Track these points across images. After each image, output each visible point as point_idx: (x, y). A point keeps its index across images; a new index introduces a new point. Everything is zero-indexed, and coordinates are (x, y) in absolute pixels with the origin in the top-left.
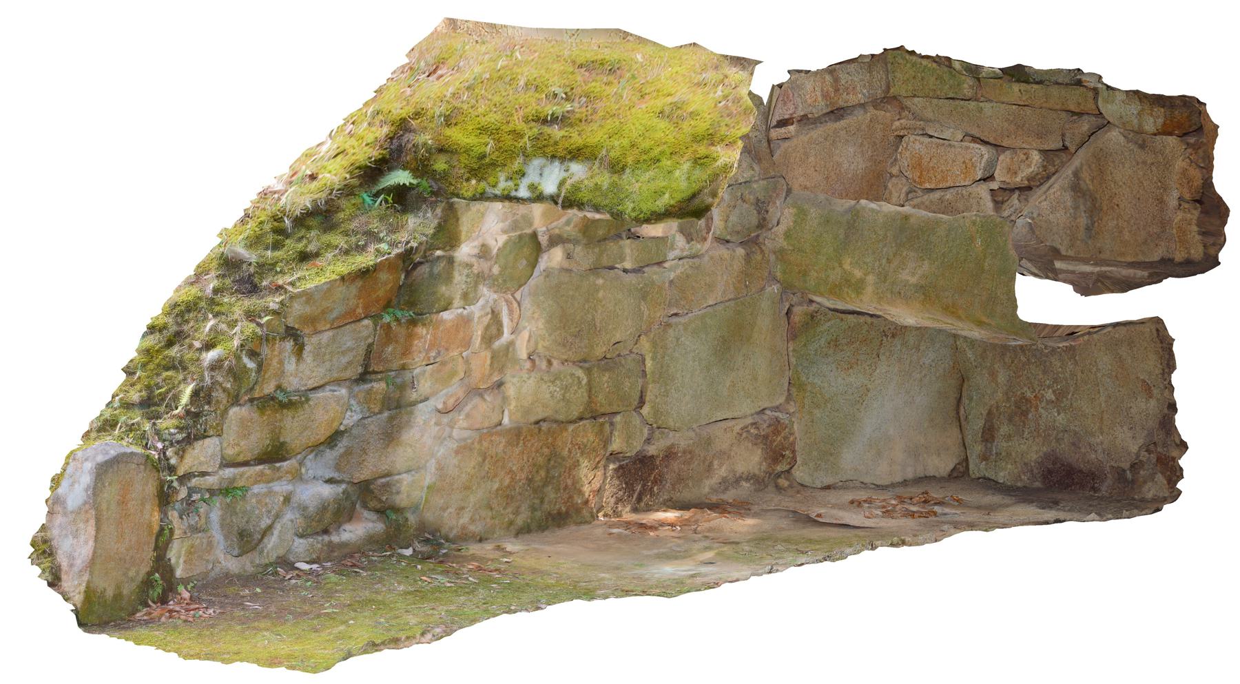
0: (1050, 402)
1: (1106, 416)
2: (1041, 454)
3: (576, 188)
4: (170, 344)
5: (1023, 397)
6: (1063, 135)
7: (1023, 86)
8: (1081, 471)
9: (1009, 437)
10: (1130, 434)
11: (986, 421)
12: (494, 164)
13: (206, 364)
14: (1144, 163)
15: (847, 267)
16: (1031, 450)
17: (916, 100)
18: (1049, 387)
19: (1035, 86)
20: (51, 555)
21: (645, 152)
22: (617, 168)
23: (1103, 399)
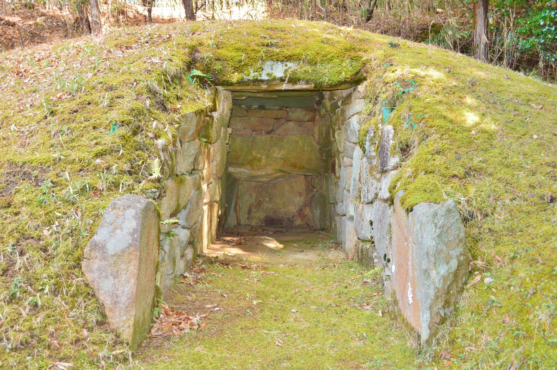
3: (294, 73)
4: (135, 133)
5: (260, 201)
7: (265, 111)
9: (255, 212)
12: (246, 65)
13: (160, 147)
15: (254, 154)
16: (261, 215)
20: (93, 296)
21: (324, 56)
22: (312, 63)
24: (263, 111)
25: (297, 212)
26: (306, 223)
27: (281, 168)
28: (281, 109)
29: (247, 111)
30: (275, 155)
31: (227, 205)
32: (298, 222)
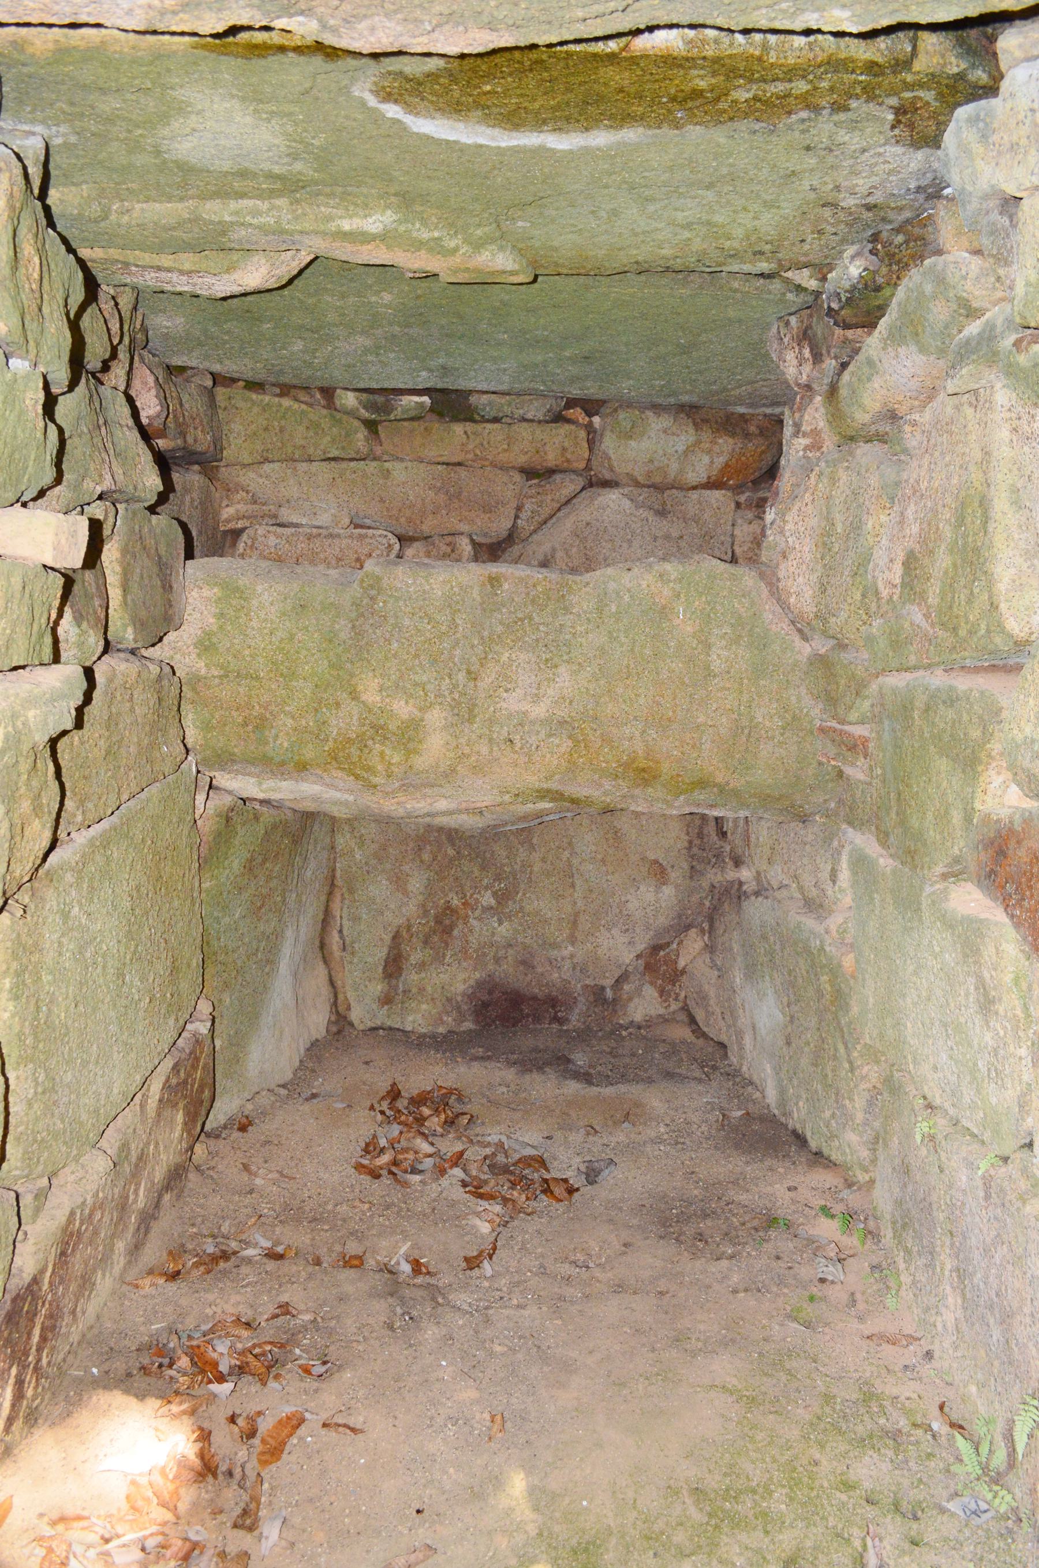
1: (582, 918)
2: (472, 982)
5: (448, 907)
6: (519, 509)
7: (470, 427)
8: (534, 998)
9: (422, 966)
10: (624, 939)
11: (391, 948)
14: (667, 537)
15: (372, 697)
16: (457, 978)
17: (267, 467)
18: (486, 888)
19: (489, 426)
23: (578, 894)
24: (458, 428)
27: (553, 785)
28: (558, 418)
29: (371, 426)
30: (513, 702)
32: (644, 1004)
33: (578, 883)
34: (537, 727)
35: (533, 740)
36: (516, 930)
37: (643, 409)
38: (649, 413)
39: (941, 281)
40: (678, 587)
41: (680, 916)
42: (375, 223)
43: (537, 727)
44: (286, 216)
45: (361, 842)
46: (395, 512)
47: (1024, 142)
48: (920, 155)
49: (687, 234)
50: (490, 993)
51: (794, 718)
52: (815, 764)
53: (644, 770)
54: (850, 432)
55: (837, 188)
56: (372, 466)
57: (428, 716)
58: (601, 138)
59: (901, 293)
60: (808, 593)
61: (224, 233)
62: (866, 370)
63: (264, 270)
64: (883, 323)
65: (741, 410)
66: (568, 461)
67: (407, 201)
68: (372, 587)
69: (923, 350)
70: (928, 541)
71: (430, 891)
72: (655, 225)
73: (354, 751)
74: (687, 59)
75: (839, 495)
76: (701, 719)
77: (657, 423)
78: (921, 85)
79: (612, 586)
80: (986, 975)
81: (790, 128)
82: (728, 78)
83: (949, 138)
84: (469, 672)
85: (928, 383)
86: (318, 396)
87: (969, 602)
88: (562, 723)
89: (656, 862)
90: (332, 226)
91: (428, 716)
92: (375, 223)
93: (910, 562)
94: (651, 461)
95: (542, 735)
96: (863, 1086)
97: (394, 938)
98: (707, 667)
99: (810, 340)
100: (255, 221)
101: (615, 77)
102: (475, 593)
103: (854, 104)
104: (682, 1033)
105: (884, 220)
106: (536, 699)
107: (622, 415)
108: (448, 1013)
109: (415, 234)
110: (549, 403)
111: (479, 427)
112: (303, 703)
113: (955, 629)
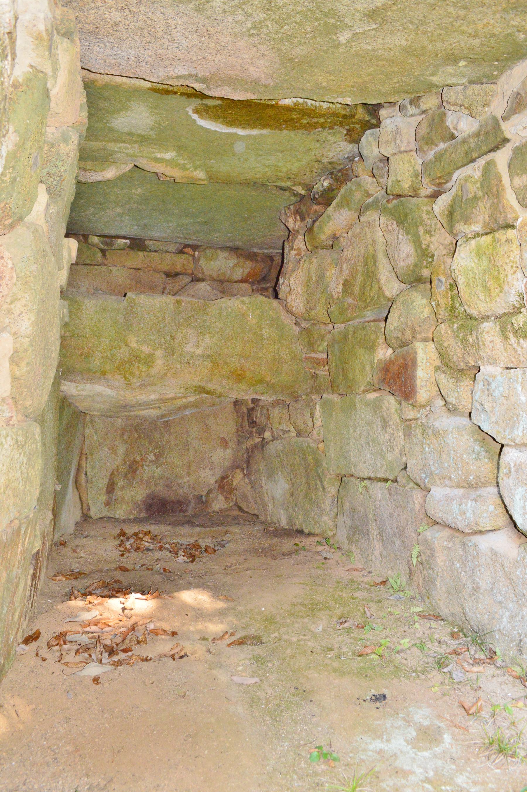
0: (151, 461)
2: (145, 495)
7: (146, 253)
9: (123, 488)
11: (110, 479)
15: (133, 344)
16: (138, 493)
18: (151, 452)
19: (153, 253)
23: (191, 454)
24: (141, 254)
25: (216, 482)
26: (236, 504)
27: (202, 384)
28: (181, 252)
29: (103, 252)
30: (189, 348)
31: (58, 488)
32: (219, 503)
33: (191, 449)
34: (198, 358)
35: (197, 363)
36: (164, 472)
37: (216, 248)
38: (219, 251)
39: (359, 185)
40: (249, 306)
41: (234, 462)
42: (168, 156)
43: (198, 358)
44: (137, 151)
45: (96, 431)
46: (113, 288)
47: (390, 140)
48: (351, 146)
49: (267, 169)
50: (153, 500)
51: (295, 355)
52: (303, 372)
53: (240, 375)
54: (317, 244)
55: (323, 155)
56: (104, 268)
57: (156, 353)
58: (255, 132)
59: (342, 191)
60: (301, 305)
61: (112, 155)
62: (326, 219)
63: (114, 172)
64: (334, 203)
65: (255, 250)
66: (185, 269)
67: (180, 149)
68: (131, 302)
69: (350, 210)
70: (353, 275)
71: (127, 453)
72: (258, 165)
73: (127, 366)
74: (293, 109)
75: (313, 267)
76: (261, 355)
77: (222, 255)
78: (357, 123)
79: (224, 305)
80: (385, 414)
81: (314, 133)
82: (303, 115)
83: (363, 139)
84: (171, 336)
85: (350, 223)
86: (81, 238)
87: (371, 289)
88: (208, 356)
89: (224, 438)
90: (154, 155)
91: (156, 353)
92: (168, 156)
93: (346, 284)
94: (219, 270)
95: (201, 361)
96: (329, 495)
97: (111, 475)
98: (262, 336)
99: (299, 213)
100: (126, 151)
101: (271, 112)
102: (172, 306)
103: (336, 127)
104: (237, 513)
105: (334, 168)
106: (198, 347)
107: (208, 251)
108: (135, 510)
109: (179, 161)
110: (177, 245)
111: (149, 254)
112: (105, 347)
113: (365, 300)
